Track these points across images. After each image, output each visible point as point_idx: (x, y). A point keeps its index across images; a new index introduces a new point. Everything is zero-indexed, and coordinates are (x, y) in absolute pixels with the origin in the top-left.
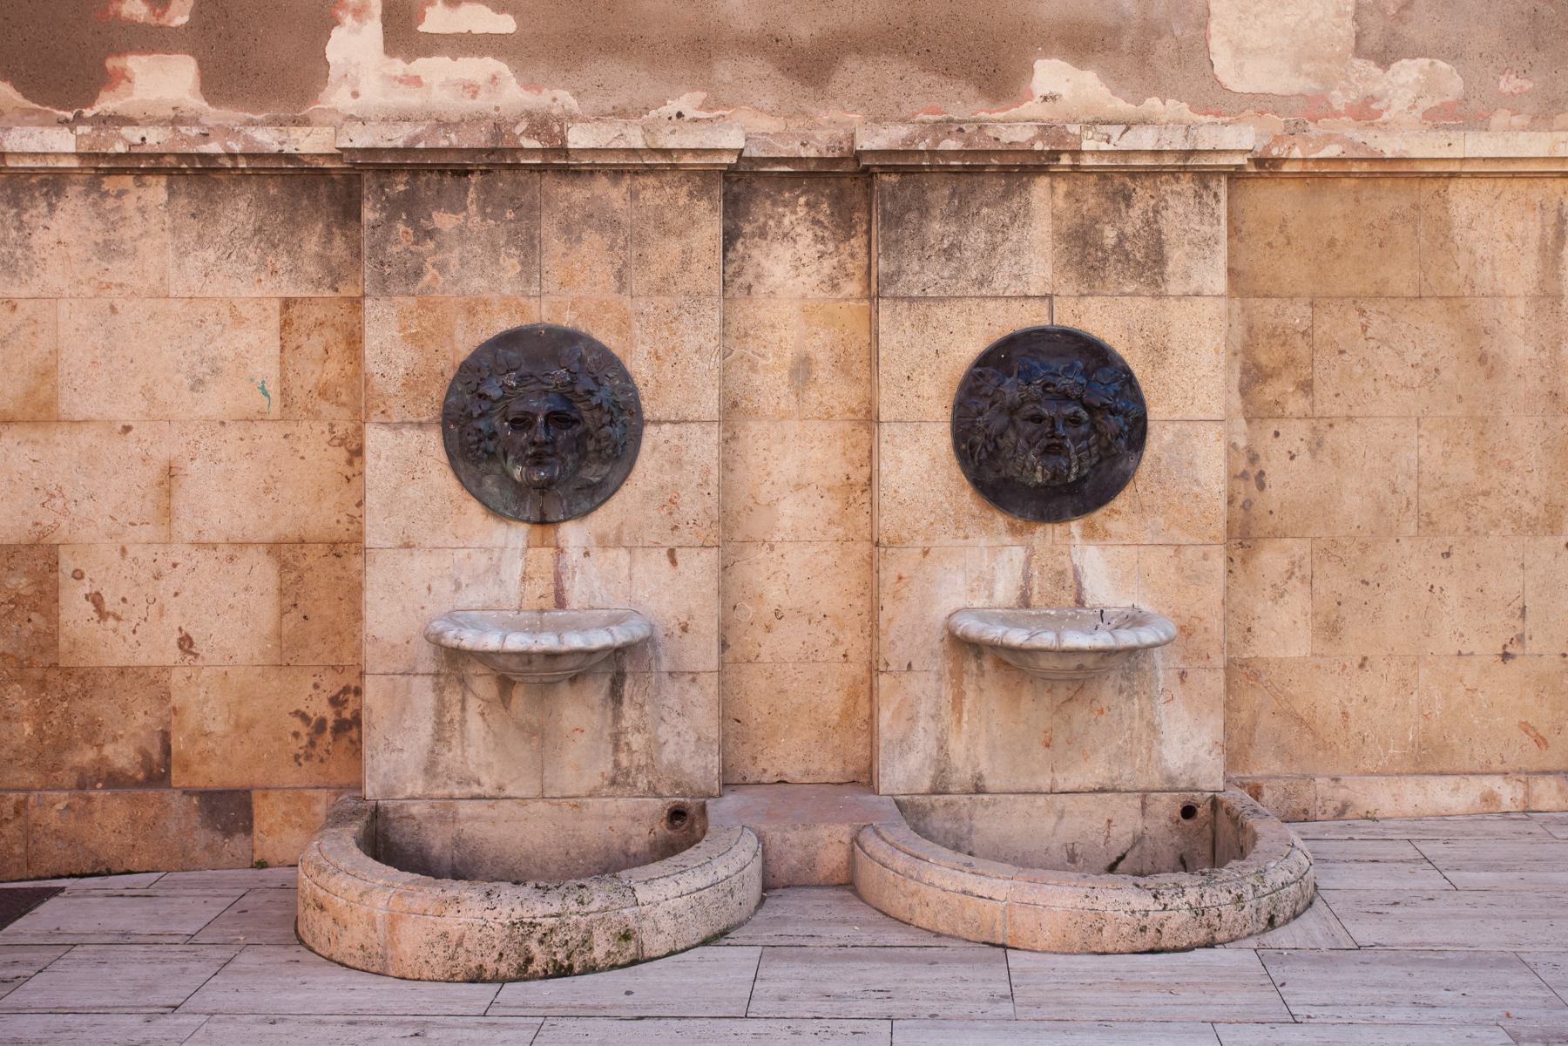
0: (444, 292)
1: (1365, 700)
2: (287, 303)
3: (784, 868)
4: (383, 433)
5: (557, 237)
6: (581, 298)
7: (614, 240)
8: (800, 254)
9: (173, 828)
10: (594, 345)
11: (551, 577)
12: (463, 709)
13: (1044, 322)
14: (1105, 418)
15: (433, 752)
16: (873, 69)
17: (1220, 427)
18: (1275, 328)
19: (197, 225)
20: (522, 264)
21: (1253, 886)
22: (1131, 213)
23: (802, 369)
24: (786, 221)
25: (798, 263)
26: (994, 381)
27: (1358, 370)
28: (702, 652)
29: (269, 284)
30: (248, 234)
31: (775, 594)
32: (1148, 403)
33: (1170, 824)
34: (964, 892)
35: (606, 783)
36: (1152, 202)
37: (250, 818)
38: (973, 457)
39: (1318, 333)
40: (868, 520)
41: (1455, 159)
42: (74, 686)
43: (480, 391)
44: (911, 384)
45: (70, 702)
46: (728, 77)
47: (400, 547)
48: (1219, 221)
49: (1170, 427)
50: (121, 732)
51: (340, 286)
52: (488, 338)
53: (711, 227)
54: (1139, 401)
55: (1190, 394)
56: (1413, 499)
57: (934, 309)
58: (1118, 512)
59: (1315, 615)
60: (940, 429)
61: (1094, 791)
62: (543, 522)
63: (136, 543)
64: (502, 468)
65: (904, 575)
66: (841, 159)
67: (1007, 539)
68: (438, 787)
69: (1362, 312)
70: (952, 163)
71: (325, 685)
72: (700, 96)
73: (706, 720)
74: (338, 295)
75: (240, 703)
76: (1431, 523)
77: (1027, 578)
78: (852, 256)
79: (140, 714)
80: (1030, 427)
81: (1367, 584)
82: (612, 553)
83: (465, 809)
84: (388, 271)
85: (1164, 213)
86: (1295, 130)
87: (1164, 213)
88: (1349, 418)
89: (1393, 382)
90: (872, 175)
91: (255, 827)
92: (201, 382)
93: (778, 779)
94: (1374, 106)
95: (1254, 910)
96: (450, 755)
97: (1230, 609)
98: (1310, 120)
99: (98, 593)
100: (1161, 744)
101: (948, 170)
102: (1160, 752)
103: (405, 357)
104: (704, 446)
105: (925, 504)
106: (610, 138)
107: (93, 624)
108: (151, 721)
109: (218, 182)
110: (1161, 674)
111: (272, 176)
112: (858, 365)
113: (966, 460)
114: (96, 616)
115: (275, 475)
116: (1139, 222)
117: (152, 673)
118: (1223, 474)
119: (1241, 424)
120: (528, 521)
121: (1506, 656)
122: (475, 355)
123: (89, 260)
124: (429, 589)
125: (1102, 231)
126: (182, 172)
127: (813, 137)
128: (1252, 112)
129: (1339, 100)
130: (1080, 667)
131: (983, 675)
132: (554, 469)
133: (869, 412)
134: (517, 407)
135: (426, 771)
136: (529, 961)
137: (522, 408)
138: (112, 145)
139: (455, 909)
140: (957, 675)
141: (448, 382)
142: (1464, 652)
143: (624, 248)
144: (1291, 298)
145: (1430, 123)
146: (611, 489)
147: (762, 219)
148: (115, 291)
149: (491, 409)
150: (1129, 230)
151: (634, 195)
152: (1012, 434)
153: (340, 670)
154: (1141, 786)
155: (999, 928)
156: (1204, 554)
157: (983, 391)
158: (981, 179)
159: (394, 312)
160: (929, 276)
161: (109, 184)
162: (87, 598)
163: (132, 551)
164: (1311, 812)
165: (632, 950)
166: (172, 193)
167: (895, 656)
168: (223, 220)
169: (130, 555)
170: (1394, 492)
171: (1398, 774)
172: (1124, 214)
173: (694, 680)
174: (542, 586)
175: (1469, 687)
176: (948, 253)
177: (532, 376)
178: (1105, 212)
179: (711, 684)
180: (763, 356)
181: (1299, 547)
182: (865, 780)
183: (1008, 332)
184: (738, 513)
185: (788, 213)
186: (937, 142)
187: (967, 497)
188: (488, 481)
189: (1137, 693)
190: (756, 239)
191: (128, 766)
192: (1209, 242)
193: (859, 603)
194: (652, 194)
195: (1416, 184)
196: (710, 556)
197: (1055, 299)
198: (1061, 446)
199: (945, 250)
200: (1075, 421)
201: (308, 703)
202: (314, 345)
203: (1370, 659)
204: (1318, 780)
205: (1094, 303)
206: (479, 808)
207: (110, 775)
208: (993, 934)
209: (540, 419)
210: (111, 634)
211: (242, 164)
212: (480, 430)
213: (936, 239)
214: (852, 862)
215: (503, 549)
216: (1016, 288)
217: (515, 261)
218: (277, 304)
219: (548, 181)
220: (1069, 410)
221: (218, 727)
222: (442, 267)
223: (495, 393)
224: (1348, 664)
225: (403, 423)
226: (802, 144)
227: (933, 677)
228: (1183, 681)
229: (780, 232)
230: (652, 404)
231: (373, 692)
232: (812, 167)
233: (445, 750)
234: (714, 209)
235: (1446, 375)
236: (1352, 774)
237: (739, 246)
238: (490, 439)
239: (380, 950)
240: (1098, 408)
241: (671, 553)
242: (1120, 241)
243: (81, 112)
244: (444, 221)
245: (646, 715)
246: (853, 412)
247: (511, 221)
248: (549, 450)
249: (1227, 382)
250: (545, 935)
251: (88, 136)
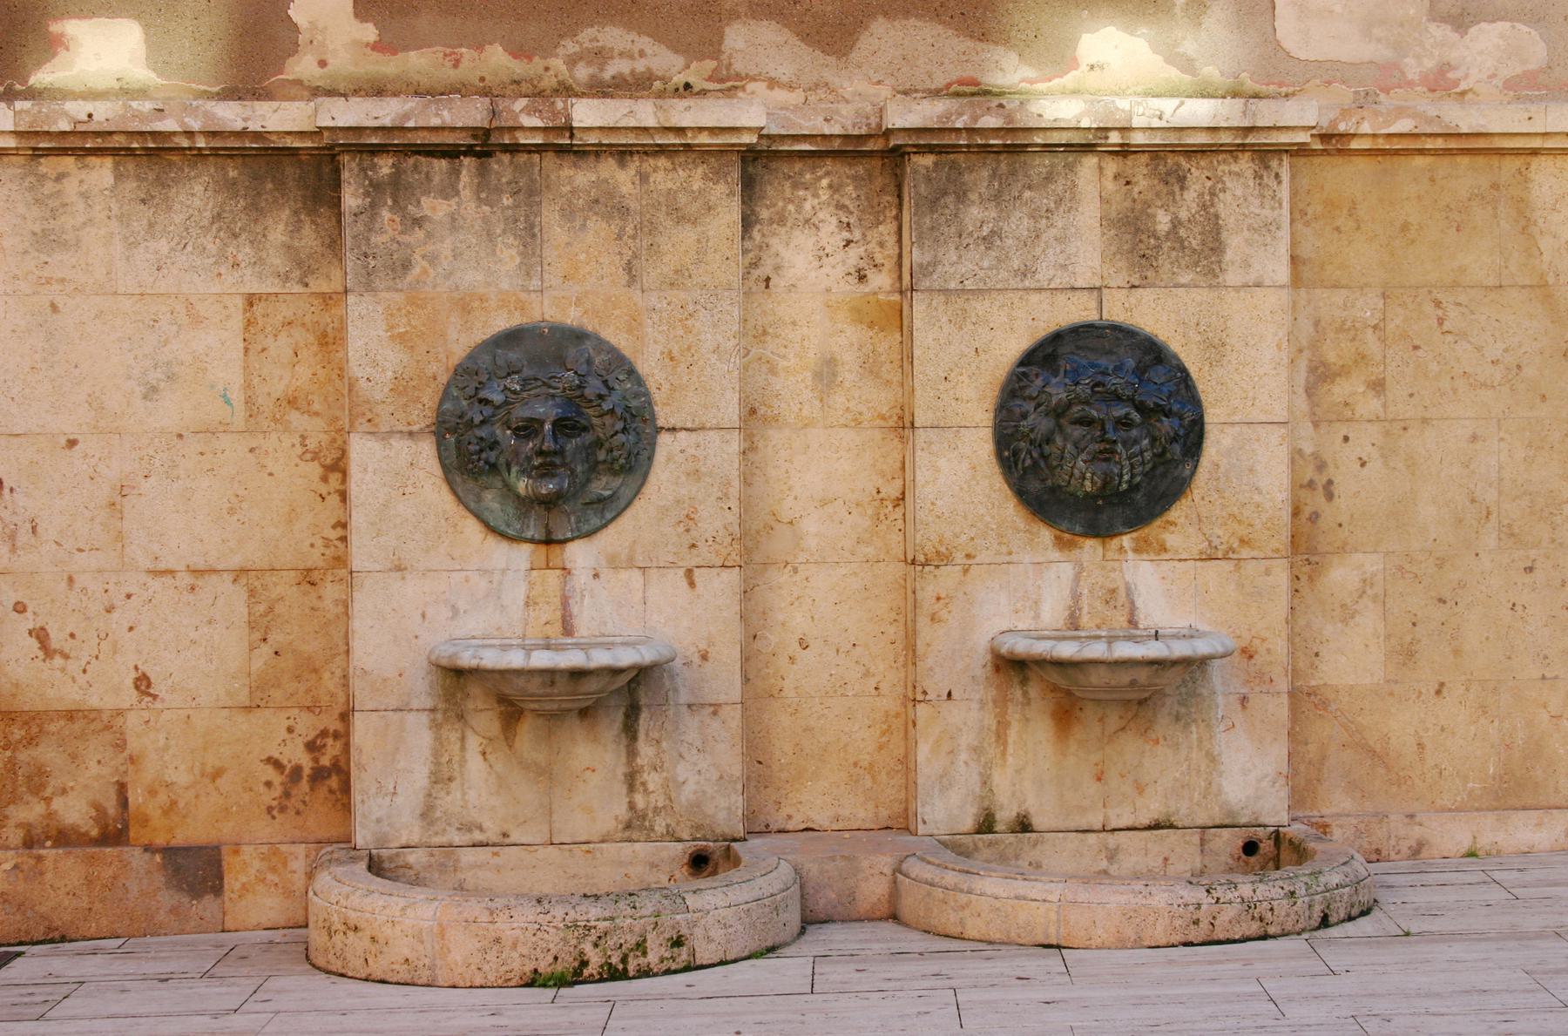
0: (435, 287)
1: (1443, 730)
2: (251, 300)
3: (822, 902)
4: (369, 444)
5: (561, 227)
6: (587, 292)
7: (623, 229)
8: (823, 243)
9: (134, 889)
10: (602, 344)
11: (557, 601)
12: (463, 748)
13: (1091, 316)
14: (1159, 421)
15: (430, 795)
16: (901, 34)
17: (1283, 431)
18: (1344, 323)
19: (146, 213)
20: (521, 254)
21: (1306, 884)
22: (1185, 196)
23: (826, 374)
24: (807, 206)
25: (821, 253)
26: (1039, 382)
27: (1434, 367)
28: (724, 682)
29: (230, 278)
30: (206, 222)
31: (798, 621)
32: (1205, 404)
33: (1230, 861)
34: (1017, 898)
35: (620, 827)
36: (1209, 184)
37: (220, 877)
38: (1016, 465)
39: (1391, 327)
40: (901, 538)
41: (1536, 134)
42: (17, 733)
43: (482, 394)
44: (948, 385)
45: (14, 751)
46: (740, 45)
47: (390, 570)
48: (1280, 204)
49: (1229, 430)
50: (71, 784)
51: (310, 280)
52: (485, 337)
53: (731, 212)
54: (1195, 402)
55: (1251, 394)
56: (1494, 509)
57: (973, 303)
58: (1173, 524)
59: (1388, 637)
60: (981, 435)
61: (1149, 828)
62: (548, 541)
63: (84, 571)
64: (504, 481)
65: (943, 596)
66: (869, 136)
67: (1055, 555)
68: (437, 833)
69: (1438, 304)
70: (992, 142)
71: (300, 728)
73: (730, 759)
74: (308, 290)
75: (205, 749)
76: (1513, 535)
77: (1076, 597)
78: (881, 244)
79: (93, 764)
80: (1077, 432)
81: (1445, 602)
82: (624, 575)
83: (468, 856)
84: (373, 263)
85: (1221, 195)
86: (1364, 101)
87: (1221, 195)
89: (1471, 380)
90: (902, 155)
91: (226, 886)
92: (154, 389)
93: (804, 826)
94: (1451, 75)
95: (1306, 906)
96: (449, 799)
97: (1295, 636)
98: (1381, 90)
99: (42, 629)
100: (1221, 776)
101: (985, 149)
102: (1220, 785)
103: (392, 359)
104: (723, 452)
105: (965, 517)
106: (619, 115)
107: (38, 663)
108: (105, 771)
109: (171, 164)
110: (1220, 700)
111: (231, 156)
112: (888, 366)
113: (1010, 468)
114: (41, 654)
115: (240, 493)
116: (1195, 205)
117: (105, 717)
118: (1286, 481)
119: (1306, 429)
120: (532, 541)
122: (472, 356)
123: (26, 252)
124: (423, 616)
125: (1154, 216)
126: (130, 152)
127: (837, 112)
128: (1318, 81)
130: (1133, 683)
131: (1029, 704)
132: (564, 481)
133: (901, 418)
134: (521, 413)
135: (423, 816)
136: (585, 964)
137: (526, 413)
138: (55, 122)
139: (507, 915)
140: (1001, 702)
141: (442, 388)
142: (1548, 675)
143: (634, 237)
144: (1362, 288)
145: (1512, 93)
146: (622, 503)
147: (780, 204)
148: (56, 287)
149: (494, 416)
150: (1184, 215)
151: (644, 178)
152: (1059, 441)
153: (318, 710)
154: (1200, 822)
155: (1052, 930)
156: (1266, 569)
157: (1027, 392)
158: (1022, 158)
159: (380, 309)
160: (967, 267)
161: (47, 166)
162: (30, 633)
163: (81, 581)
164: (1384, 853)
165: (684, 957)
166: (119, 177)
167: (936, 685)
168: (177, 207)
169: (78, 586)
170: (1473, 501)
171: (1477, 810)
172: (1178, 197)
173: (715, 713)
174: (548, 612)
175: (1552, 714)
176: (987, 241)
177: (536, 379)
178: (1158, 195)
179: (733, 716)
180: (784, 357)
181: (1372, 564)
182: (902, 823)
183: (1053, 328)
184: (758, 532)
185: (809, 197)
186: (975, 119)
187: (1010, 509)
188: (489, 496)
189: (1195, 721)
190: (775, 226)
191: (80, 822)
192: (1269, 227)
193: (891, 630)
194: (664, 177)
195: (1495, 160)
196: (732, 576)
197: (1105, 291)
198: (1113, 452)
199: (984, 239)
200: (1125, 423)
201: (281, 749)
202: (281, 347)
203: (1448, 685)
204: (1392, 817)
205: (1146, 295)
206: (483, 854)
207: (60, 832)
208: (1047, 936)
209: (548, 427)
210: (58, 673)
211: (201, 143)
212: (482, 439)
213: (974, 226)
214: (894, 893)
215: (504, 571)
216: (1061, 280)
217: (514, 252)
218: (240, 302)
219: (550, 159)
220: (1119, 411)
221: (181, 777)
222: (432, 259)
223: (498, 398)
224: (1424, 691)
225: (391, 433)
226: (826, 120)
227: (975, 706)
228: (1244, 707)
229: (801, 218)
230: (667, 409)
231: (363, 730)
232: (836, 145)
233: (442, 794)
234: (731, 194)
235: (1529, 372)
236: (1428, 811)
237: (756, 234)
238: (491, 449)
239: (427, 961)
240: (1152, 410)
241: (689, 573)
242: (1175, 227)
243: (13, 85)
244: (434, 207)
245: (664, 752)
246: (883, 417)
247: (508, 207)
248: (558, 461)
249: (1291, 379)
250: (600, 937)
251: (27, 112)
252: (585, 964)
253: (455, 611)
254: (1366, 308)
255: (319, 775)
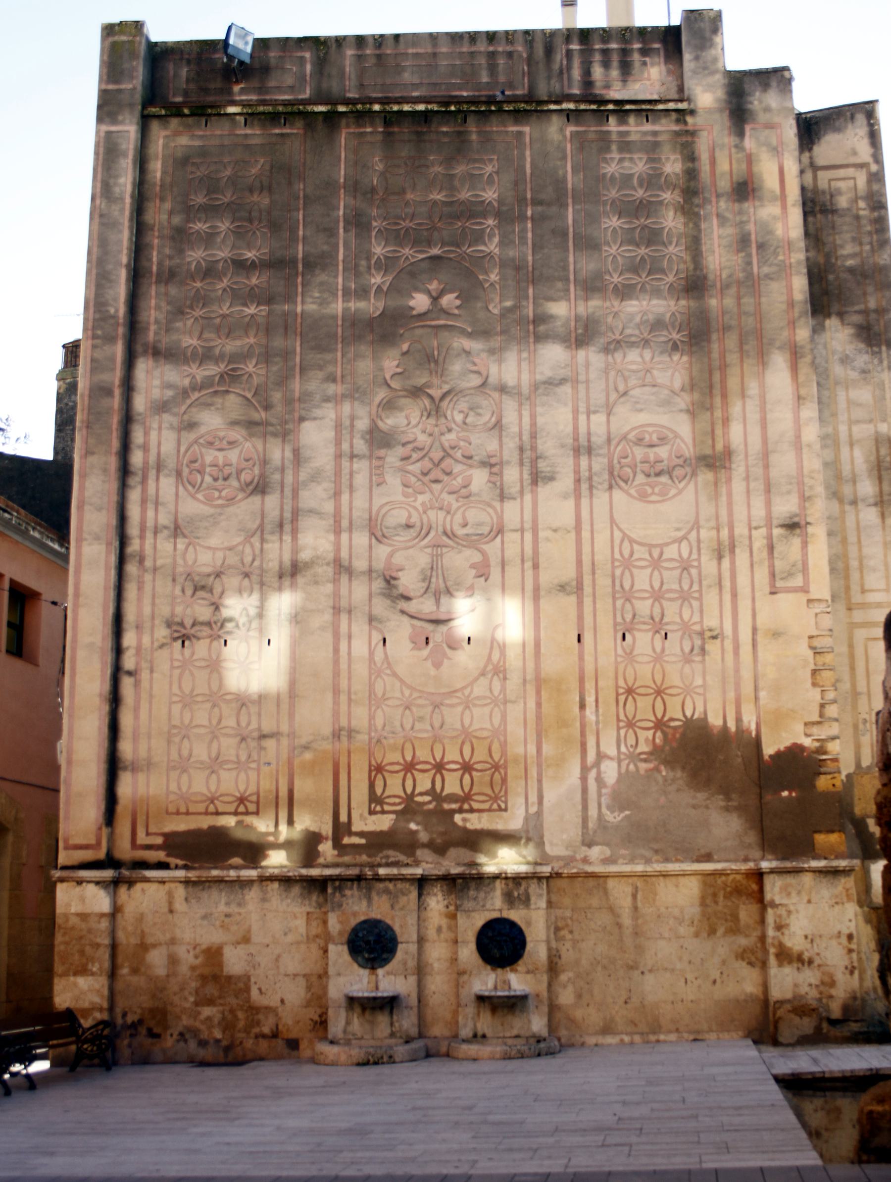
129: (578, 857)
181: (571, 974)
254: (568, 914)
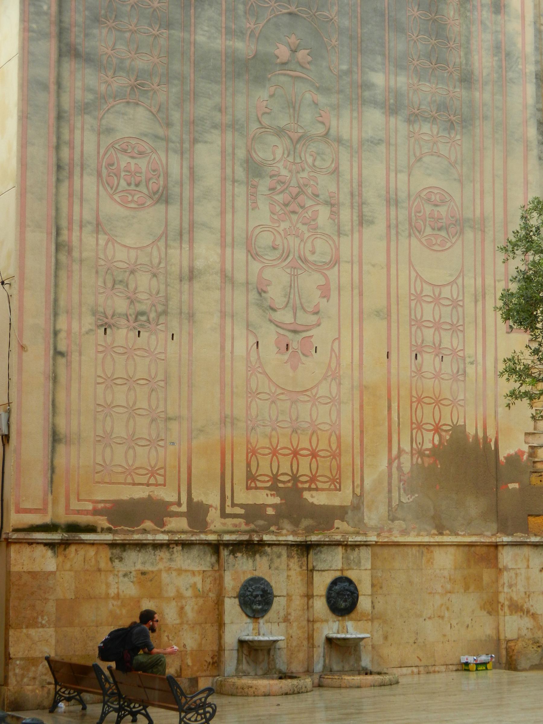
72: (277, 527)
77: (339, 627)
88: (388, 594)
121: (415, 643)
202: (208, 581)
252: (294, 691)
253: (241, 631)
255: (214, 663)
